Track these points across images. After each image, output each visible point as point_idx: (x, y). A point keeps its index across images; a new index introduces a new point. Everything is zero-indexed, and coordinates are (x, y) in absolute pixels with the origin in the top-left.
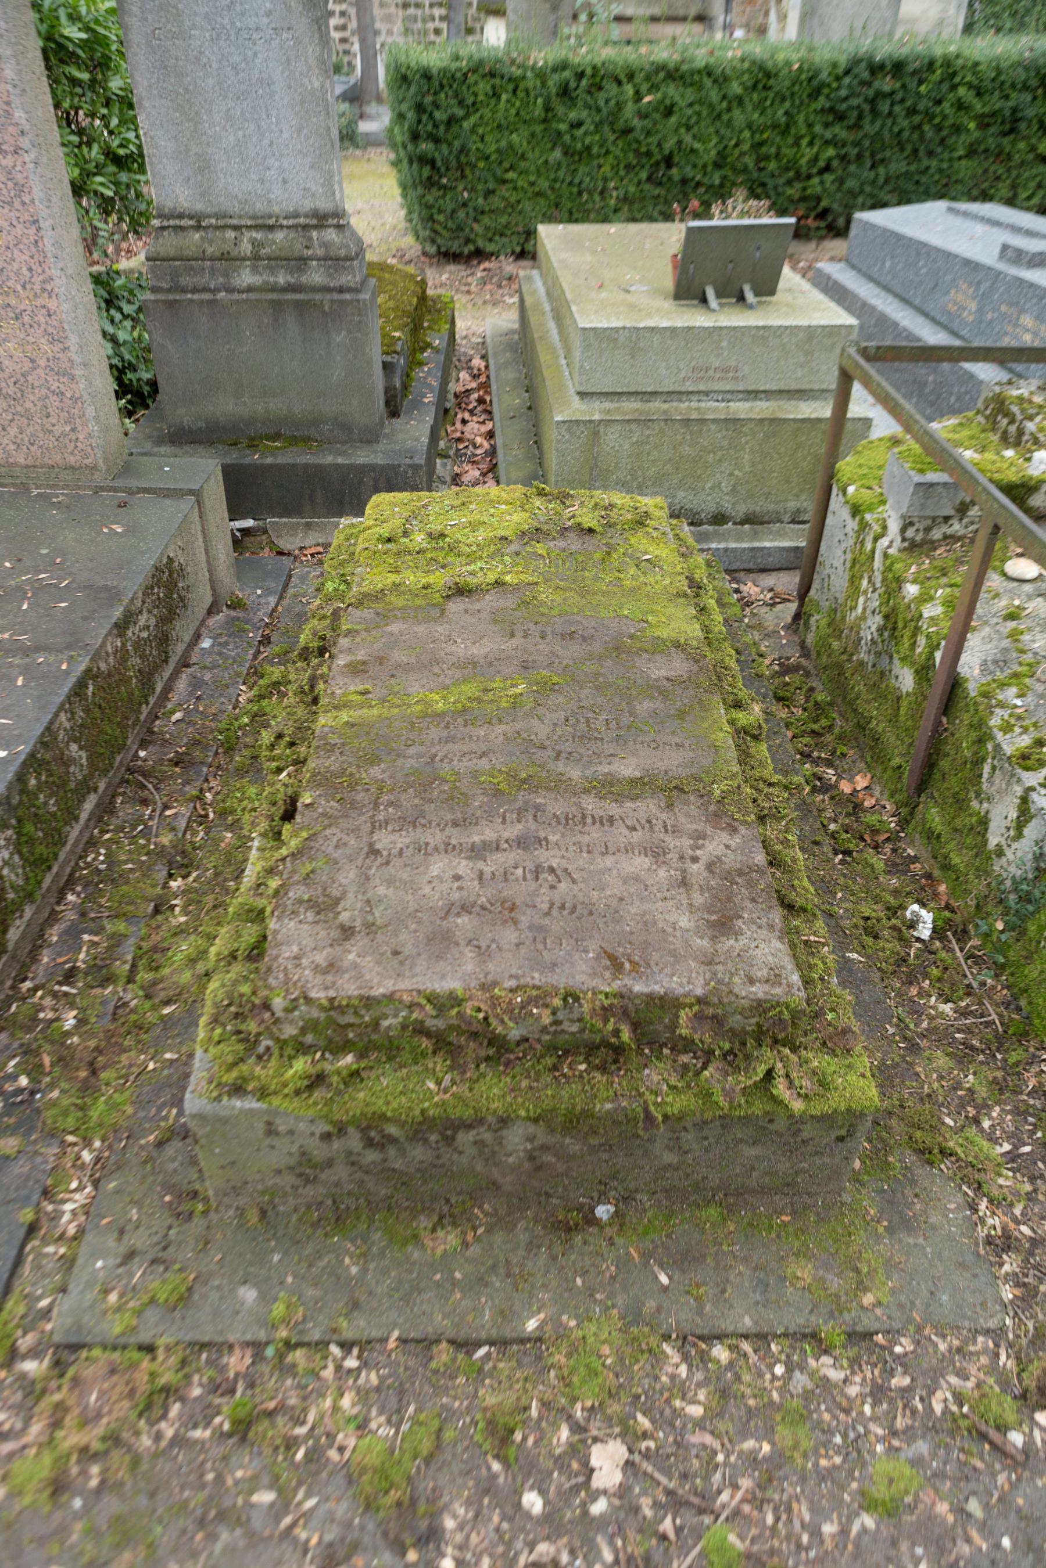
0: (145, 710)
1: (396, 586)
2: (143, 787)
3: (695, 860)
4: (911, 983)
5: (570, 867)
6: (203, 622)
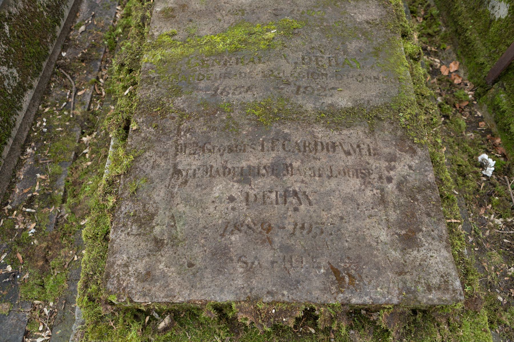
0: (59, 30)
2: (65, 77)
3: (389, 180)
4: (481, 206)
5: (308, 191)
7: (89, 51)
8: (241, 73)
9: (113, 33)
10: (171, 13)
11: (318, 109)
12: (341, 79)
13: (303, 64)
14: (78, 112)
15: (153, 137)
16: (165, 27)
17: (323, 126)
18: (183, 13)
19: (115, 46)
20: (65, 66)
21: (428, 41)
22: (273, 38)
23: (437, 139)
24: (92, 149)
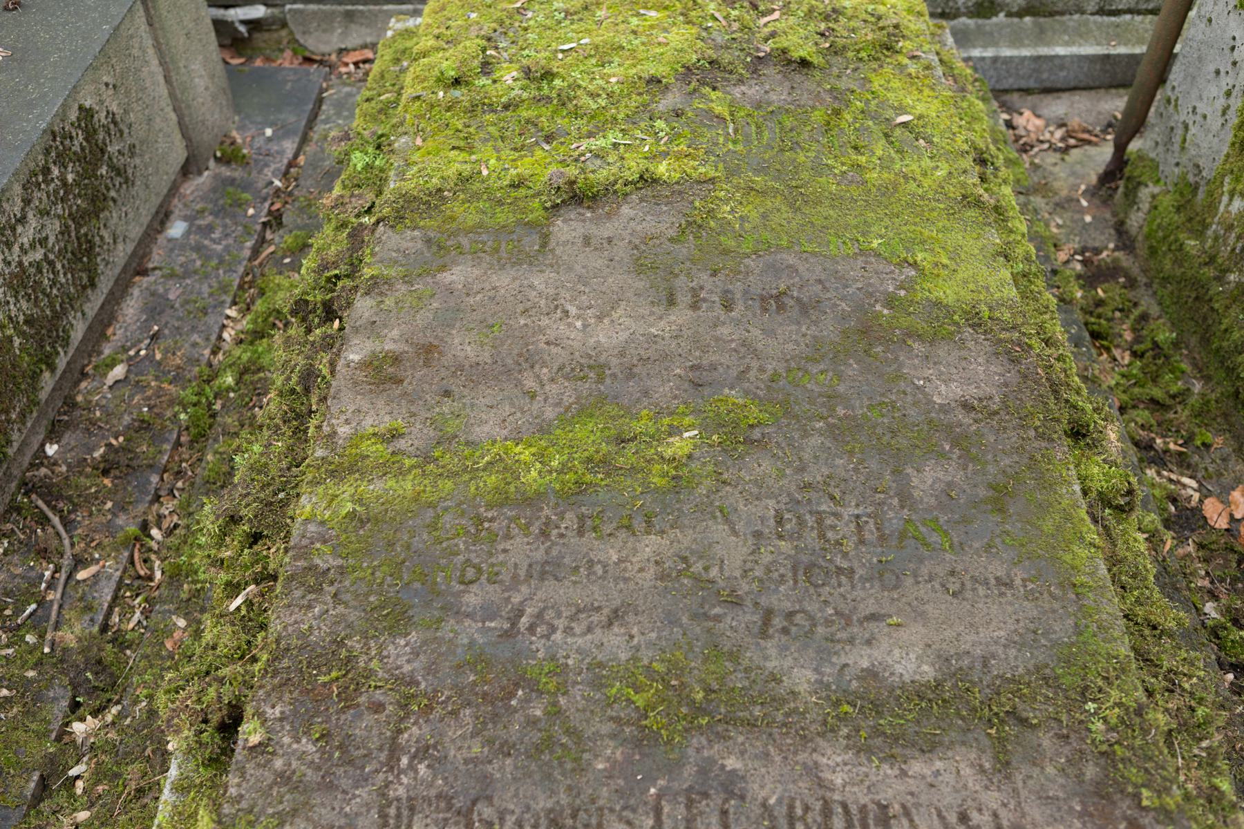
0: (48, 381)
1: (463, 180)
2: (44, 521)
6: (174, 190)
7: (128, 440)
8: (591, 563)
9: (208, 389)
10: (391, 370)
11: (828, 686)
12: (896, 587)
13: (780, 537)
14: (69, 637)
15: (309, 772)
16: (372, 412)
17: (847, 747)
18: (425, 370)
19: (210, 427)
20: (49, 487)
21: (1153, 422)
22: (690, 457)
23: (1217, 781)
24: (97, 763)
